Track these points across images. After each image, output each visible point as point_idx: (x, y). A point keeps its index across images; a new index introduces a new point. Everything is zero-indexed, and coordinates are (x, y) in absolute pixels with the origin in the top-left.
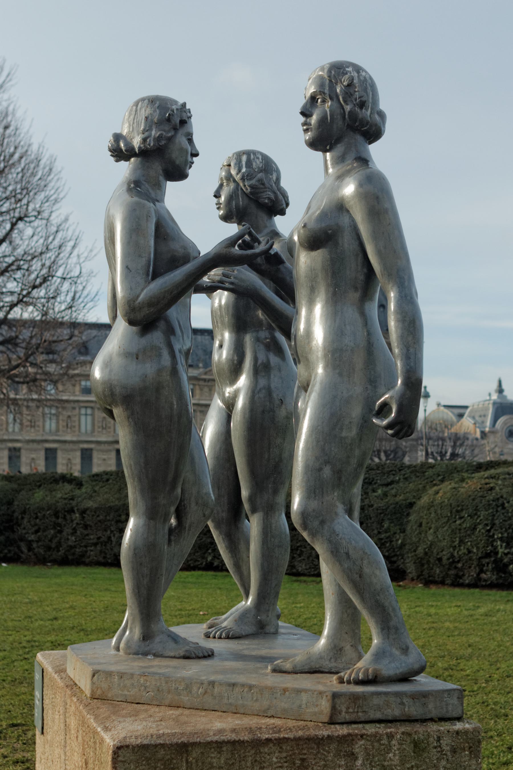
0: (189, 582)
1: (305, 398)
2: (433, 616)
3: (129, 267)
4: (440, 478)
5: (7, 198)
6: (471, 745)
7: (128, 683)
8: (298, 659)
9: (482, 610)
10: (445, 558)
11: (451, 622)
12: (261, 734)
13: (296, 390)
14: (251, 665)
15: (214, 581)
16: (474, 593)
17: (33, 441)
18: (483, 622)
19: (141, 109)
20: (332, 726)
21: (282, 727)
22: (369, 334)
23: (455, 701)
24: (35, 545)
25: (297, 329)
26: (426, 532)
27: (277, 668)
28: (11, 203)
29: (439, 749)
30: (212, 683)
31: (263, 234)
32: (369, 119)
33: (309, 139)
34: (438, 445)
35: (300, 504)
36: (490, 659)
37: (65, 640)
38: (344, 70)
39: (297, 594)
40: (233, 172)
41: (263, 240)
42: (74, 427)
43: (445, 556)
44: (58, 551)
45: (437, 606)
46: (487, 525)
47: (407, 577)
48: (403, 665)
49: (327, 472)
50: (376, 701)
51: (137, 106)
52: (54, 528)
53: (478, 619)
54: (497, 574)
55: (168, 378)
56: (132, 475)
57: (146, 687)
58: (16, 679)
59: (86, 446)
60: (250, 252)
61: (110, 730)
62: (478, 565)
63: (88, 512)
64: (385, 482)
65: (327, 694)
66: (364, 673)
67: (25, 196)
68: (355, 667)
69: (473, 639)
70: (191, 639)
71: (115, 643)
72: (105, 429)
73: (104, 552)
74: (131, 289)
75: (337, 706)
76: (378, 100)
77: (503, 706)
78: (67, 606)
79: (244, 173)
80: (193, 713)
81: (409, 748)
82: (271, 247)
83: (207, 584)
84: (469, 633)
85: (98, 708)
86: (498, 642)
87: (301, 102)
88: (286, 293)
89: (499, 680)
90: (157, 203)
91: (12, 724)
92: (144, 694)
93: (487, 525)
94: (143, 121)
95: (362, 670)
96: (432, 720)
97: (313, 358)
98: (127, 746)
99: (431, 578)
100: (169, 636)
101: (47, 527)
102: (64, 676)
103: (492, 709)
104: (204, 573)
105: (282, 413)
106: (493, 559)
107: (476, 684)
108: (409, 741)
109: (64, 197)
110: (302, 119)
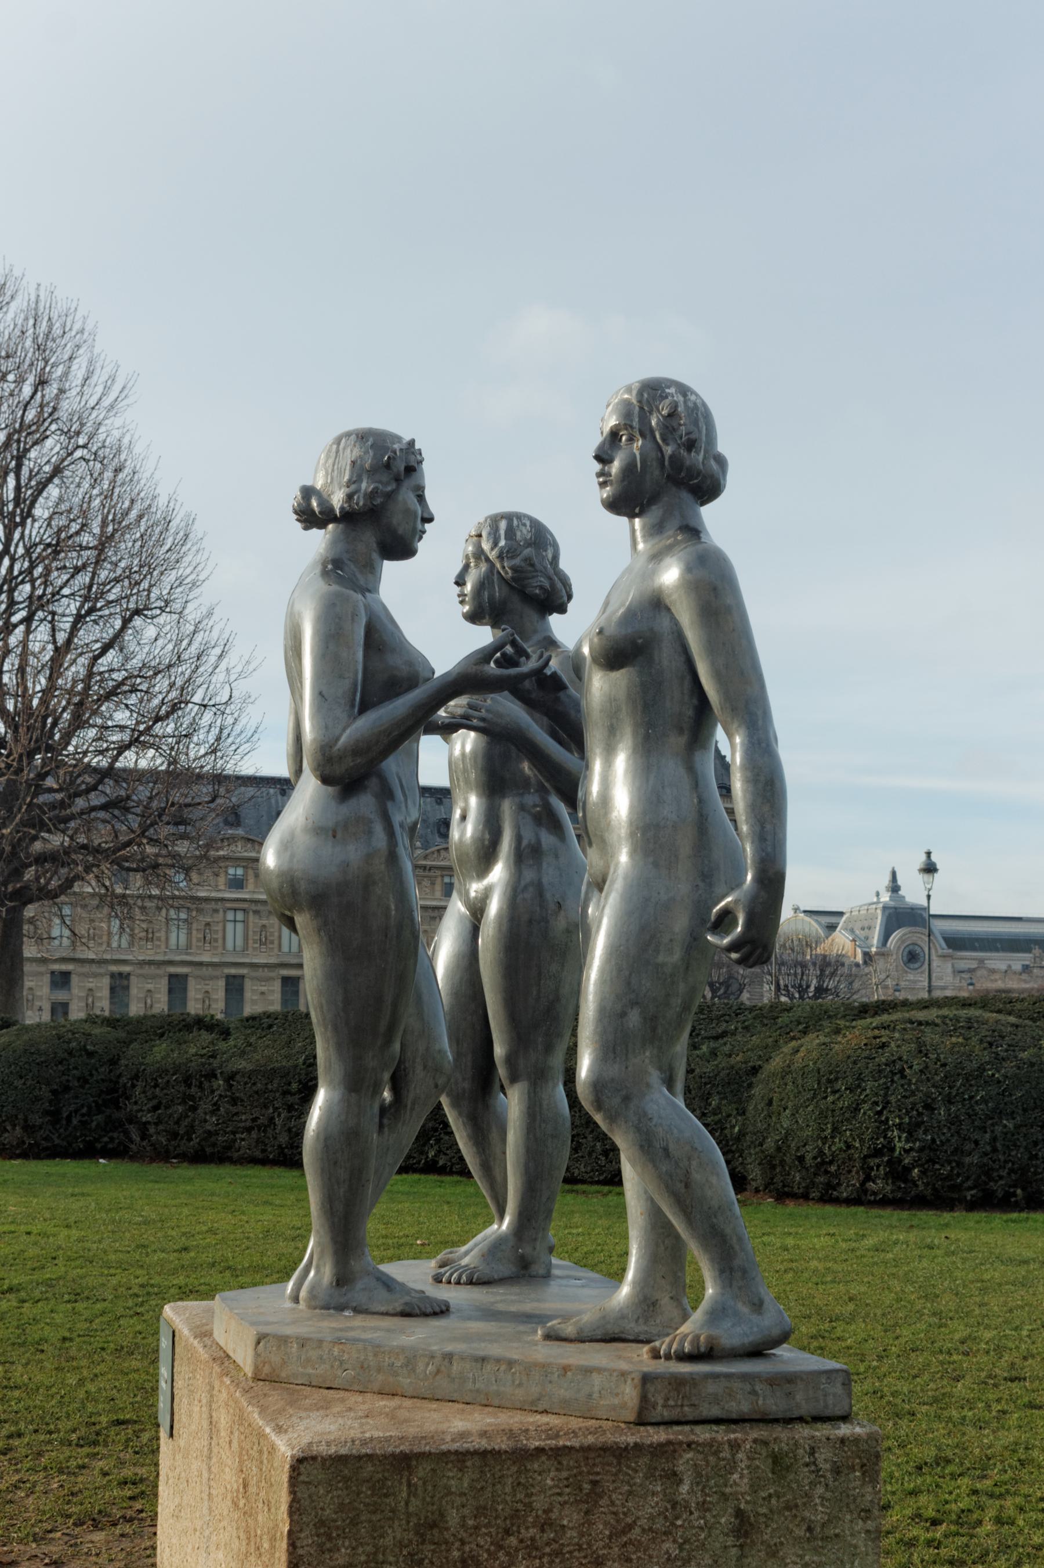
0: (398, 1192)
1: (599, 901)
2: (791, 1251)
3: (324, 693)
4: (801, 1027)
5: (117, 580)
6: (865, 1461)
7: (313, 1354)
8: (586, 1318)
9: (870, 1242)
10: (809, 1157)
11: (820, 1260)
12: (527, 1440)
13: (584, 888)
14: (509, 1328)
15: (438, 1190)
16: (856, 1213)
17: (150, 963)
18: (871, 1260)
19: (344, 449)
20: (642, 1428)
21: (561, 1429)
22: (701, 801)
23: (838, 1389)
24: (152, 1130)
25: (587, 793)
26: (779, 1114)
27: (552, 1333)
28: (122, 587)
29: (813, 1468)
30: (449, 1357)
31: (531, 643)
32: (701, 467)
33: (608, 497)
34: (795, 974)
35: (591, 1070)
36: (885, 1321)
37: (201, 1284)
38: (664, 391)
39: (573, 1212)
40: (486, 546)
41: (534, 652)
42: (216, 940)
43: (810, 1153)
44: (190, 1140)
45: (797, 1233)
46: (876, 1103)
47: (748, 1187)
48: (755, 1329)
49: (634, 1018)
50: (711, 1388)
51: (339, 444)
52: (184, 1102)
53: (863, 1256)
54: (893, 1183)
55: (383, 867)
56: (324, 1020)
57: (341, 1362)
58: (122, 1348)
59: (233, 971)
60: (513, 671)
61: (286, 1431)
62: (862, 1168)
63: (238, 1077)
64: (714, 1033)
65: (633, 1375)
66: (692, 1343)
67: (145, 576)
68: (678, 1332)
69: (855, 1289)
70: (411, 1285)
71: (292, 1290)
72: (265, 944)
73: (263, 1142)
74: (326, 727)
75: (650, 1396)
76: (716, 438)
77: (906, 1399)
78: (205, 1228)
79: (502, 547)
80: (418, 1405)
81: (764, 1466)
82: (547, 664)
83: (427, 1195)
84: (848, 1279)
85: (265, 1395)
86: (896, 1293)
87: (596, 440)
88: (569, 736)
89: (899, 1356)
90: (367, 594)
91: (117, 1420)
92: (339, 1373)
93: (876, 1103)
94: (348, 468)
95: (689, 1338)
96: (801, 1419)
97: (612, 838)
98: (314, 1458)
99: (786, 1189)
100: (378, 1279)
101: (172, 1101)
102: (209, 1343)
103: (889, 1403)
104: (423, 1177)
105: (560, 924)
106: (886, 1159)
107: (862, 1361)
108: (764, 1454)
109: (207, 578)
110: (597, 467)
